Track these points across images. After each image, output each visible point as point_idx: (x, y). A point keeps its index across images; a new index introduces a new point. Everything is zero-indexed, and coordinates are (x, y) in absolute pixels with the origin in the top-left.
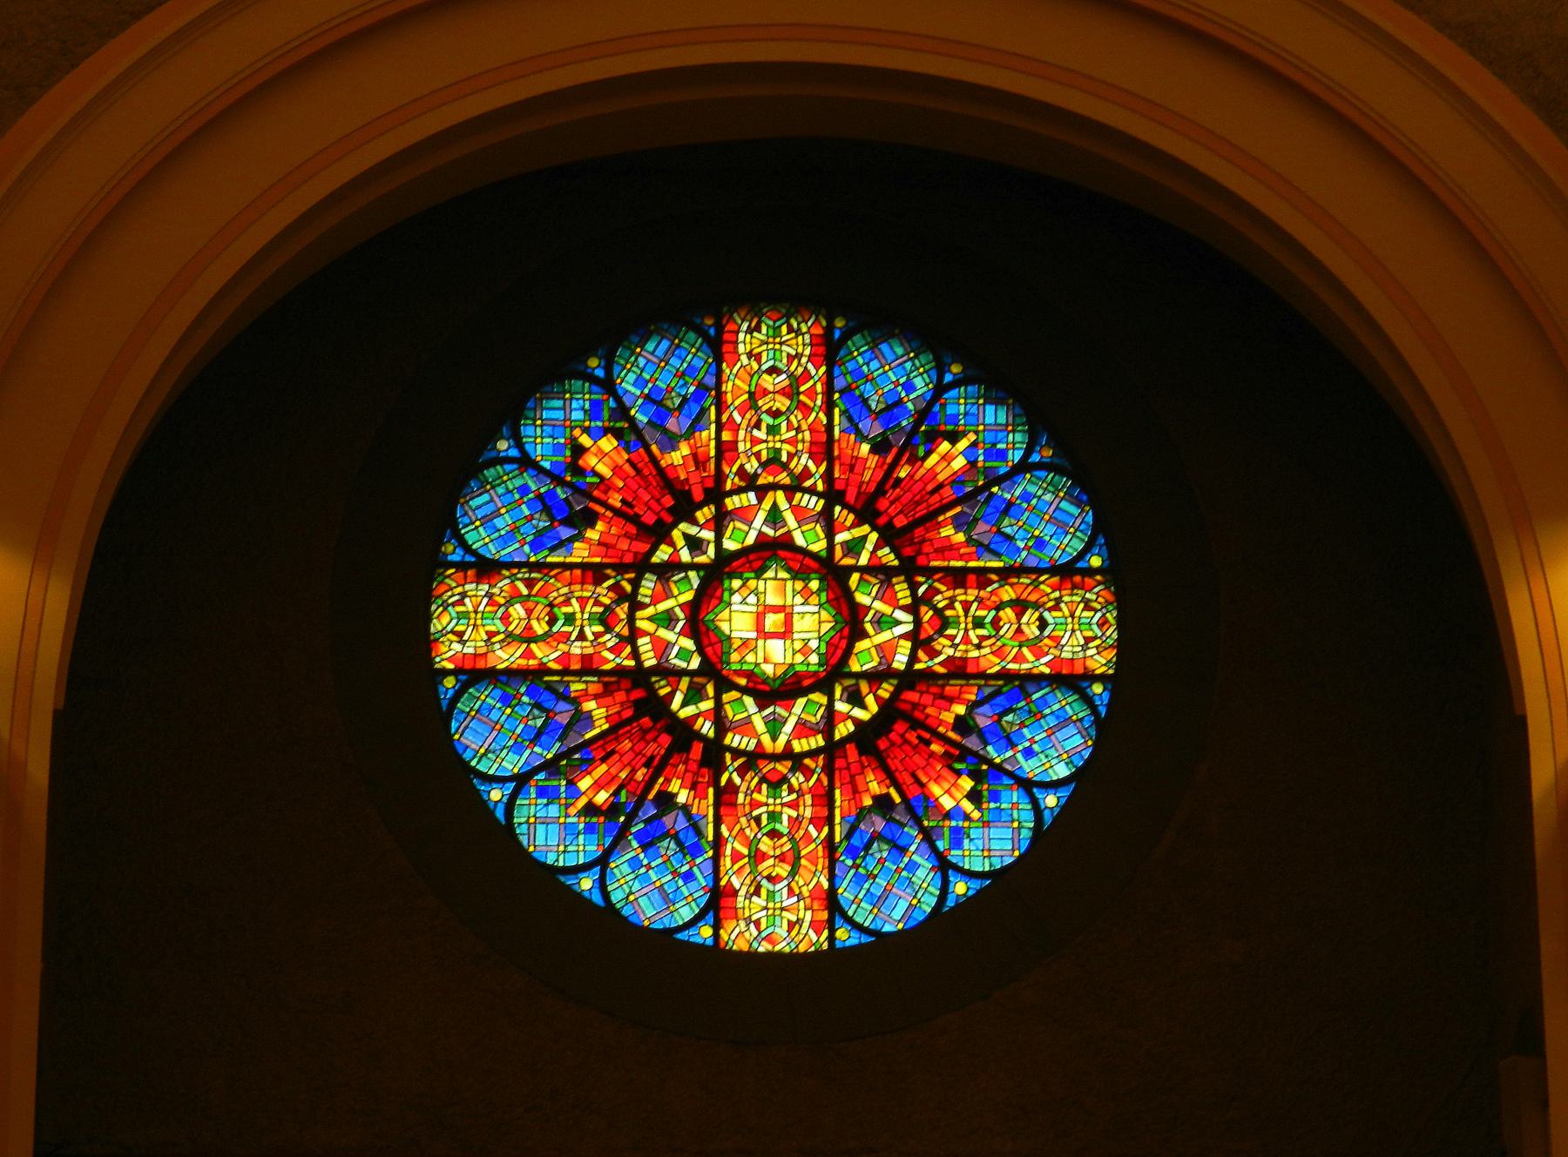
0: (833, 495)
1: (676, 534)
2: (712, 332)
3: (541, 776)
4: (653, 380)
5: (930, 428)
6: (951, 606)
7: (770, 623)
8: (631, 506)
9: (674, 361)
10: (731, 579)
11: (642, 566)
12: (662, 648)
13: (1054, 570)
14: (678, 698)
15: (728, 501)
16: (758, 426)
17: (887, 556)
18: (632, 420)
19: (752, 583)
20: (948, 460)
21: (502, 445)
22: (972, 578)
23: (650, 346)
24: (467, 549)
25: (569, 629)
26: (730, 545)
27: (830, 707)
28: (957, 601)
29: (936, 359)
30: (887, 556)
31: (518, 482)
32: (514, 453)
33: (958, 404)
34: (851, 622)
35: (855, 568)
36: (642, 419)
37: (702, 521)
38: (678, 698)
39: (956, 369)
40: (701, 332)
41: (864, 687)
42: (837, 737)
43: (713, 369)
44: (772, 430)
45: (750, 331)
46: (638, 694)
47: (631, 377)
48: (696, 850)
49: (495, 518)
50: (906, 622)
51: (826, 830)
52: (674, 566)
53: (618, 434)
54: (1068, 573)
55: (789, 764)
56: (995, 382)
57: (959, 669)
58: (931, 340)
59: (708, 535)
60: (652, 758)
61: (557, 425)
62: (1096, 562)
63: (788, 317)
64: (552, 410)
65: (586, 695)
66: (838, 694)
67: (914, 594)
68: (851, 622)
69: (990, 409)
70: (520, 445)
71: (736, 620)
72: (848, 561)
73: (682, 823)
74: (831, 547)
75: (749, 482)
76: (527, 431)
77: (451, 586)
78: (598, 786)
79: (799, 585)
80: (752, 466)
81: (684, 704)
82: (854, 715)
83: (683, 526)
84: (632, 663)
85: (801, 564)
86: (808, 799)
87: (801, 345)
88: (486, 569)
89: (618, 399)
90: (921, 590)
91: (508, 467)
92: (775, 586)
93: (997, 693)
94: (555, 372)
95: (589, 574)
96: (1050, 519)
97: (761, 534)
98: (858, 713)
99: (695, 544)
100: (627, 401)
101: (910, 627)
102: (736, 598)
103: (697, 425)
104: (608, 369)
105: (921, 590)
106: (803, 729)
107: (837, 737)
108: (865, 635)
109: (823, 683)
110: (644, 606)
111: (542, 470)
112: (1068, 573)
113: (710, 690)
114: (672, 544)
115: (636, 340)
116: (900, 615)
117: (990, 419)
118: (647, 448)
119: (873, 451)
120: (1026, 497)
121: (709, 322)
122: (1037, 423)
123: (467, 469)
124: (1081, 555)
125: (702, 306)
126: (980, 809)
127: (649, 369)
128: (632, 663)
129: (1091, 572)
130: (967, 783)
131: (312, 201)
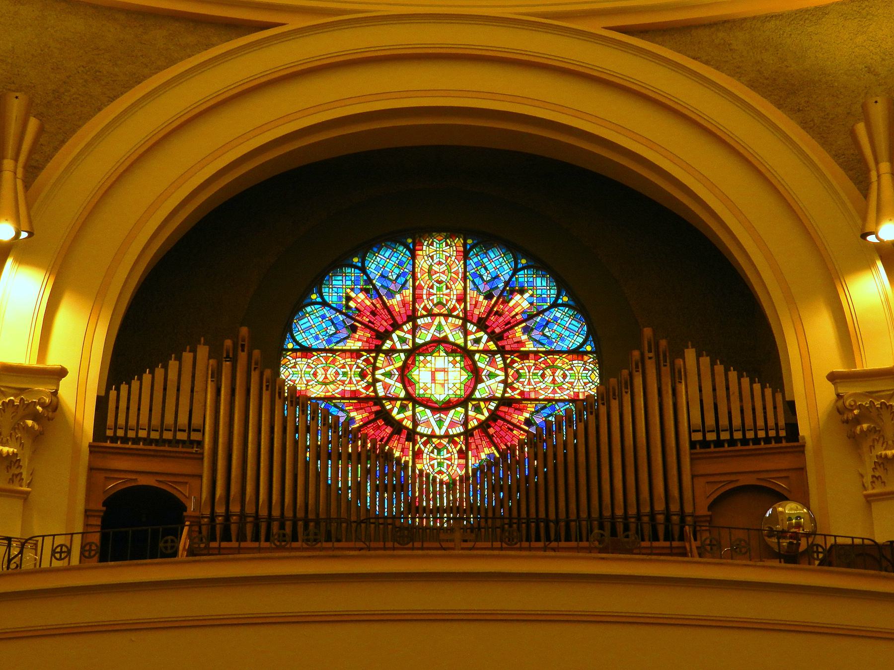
0: (466, 319)
1: (487, 414)
2: (411, 246)
3: (545, 307)
4: (384, 267)
5: (512, 289)
6: (358, 382)
7: (439, 377)
8: (373, 323)
9: (394, 259)
10: (420, 355)
11: (378, 350)
12: (386, 387)
13: (569, 352)
14: (395, 411)
15: (462, 430)
16: (432, 287)
17: (492, 346)
18: (374, 286)
19: (451, 392)
20: (520, 303)
21: (314, 297)
22: (532, 356)
23: (382, 252)
24: (297, 343)
25: (345, 378)
26: (461, 410)
27: (414, 337)
28: (524, 367)
29: (514, 257)
30: (492, 346)
31: (321, 313)
32: (319, 300)
33: (522, 277)
34: (476, 375)
35: (478, 351)
36: (378, 284)
37: (406, 330)
38: (395, 411)
39: (524, 261)
40: (406, 246)
41: (482, 404)
42: (470, 427)
43: (411, 262)
44: (439, 289)
45: (428, 245)
46: (375, 409)
47: (373, 266)
48: (474, 275)
49: (311, 327)
50: (378, 375)
51: (417, 284)
52: (393, 350)
53: (367, 291)
54: (577, 353)
55: (447, 440)
56: (539, 265)
57: (525, 397)
58: (513, 248)
59: (409, 336)
60: (383, 438)
61: (340, 287)
62: (589, 348)
63: (446, 238)
64: (337, 282)
65: (351, 411)
66: (470, 408)
67: (505, 362)
68: (476, 375)
69: (539, 280)
70: (322, 297)
71: (421, 375)
72: (474, 348)
73: (481, 288)
74: (414, 408)
75: (451, 439)
76: (325, 290)
77: (289, 359)
78: (517, 305)
79: (451, 359)
80: (451, 447)
81: (398, 413)
82: (476, 418)
83: (398, 332)
84: (373, 394)
85: (454, 349)
86: (425, 297)
87: (452, 251)
88: (306, 351)
89: (368, 276)
90: (508, 361)
91: (317, 306)
92: (440, 360)
93: (544, 408)
94: (338, 264)
95: (355, 355)
96: (568, 330)
97: (446, 415)
98: (401, 334)
99: (403, 341)
100: (371, 276)
101: (377, 372)
102: (458, 386)
103: (403, 286)
104: (363, 263)
105: (508, 361)
106: (452, 424)
107: (470, 427)
108: (398, 369)
109: (463, 402)
110: (379, 368)
111: (332, 308)
112: (577, 353)
113: (410, 405)
114: (392, 340)
115: (375, 249)
116: (498, 372)
117: (539, 284)
118: (381, 297)
119: (485, 298)
120: (556, 319)
121: (410, 241)
122: (562, 285)
123: (298, 306)
124: (582, 345)
125: (409, 233)
126: (346, 293)
127: (384, 262)
128: (373, 394)
129: (587, 353)
130: (352, 304)
131: (214, 172)
